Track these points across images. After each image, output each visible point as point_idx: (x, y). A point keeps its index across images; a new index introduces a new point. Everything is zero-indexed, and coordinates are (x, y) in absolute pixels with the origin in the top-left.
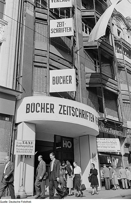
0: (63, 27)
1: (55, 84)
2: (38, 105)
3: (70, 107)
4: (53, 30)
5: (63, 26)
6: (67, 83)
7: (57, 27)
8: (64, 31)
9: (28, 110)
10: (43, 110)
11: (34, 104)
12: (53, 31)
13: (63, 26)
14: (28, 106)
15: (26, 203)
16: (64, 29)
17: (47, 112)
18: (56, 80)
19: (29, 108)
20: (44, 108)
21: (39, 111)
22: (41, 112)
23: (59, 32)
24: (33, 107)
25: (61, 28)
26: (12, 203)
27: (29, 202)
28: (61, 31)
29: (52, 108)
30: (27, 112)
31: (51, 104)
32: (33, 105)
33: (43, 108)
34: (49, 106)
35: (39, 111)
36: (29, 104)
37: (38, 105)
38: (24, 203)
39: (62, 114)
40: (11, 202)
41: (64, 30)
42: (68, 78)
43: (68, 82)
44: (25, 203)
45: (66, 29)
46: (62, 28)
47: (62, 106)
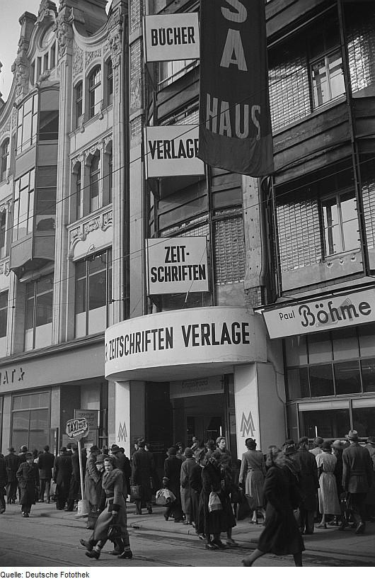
0: (181, 264)
1: (156, 44)
4: (156, 272)
5: (184, 261)
6: (184, 42)
7: (167, 261)
10: (132, 347)
12: (155, 275)
13: (184, 261)
14: (206, 328)
15: (75, 579)
16: (187, 270)
18: (158, 37)
23: (173, 280)
26: (35, 579)
27: (84, 574)
38: (68, 579)
40: (32, 575)
42: (186, 32)
43: (186, 39)
44: (71, 579)
45: (192, 268)
46: (180, 267)
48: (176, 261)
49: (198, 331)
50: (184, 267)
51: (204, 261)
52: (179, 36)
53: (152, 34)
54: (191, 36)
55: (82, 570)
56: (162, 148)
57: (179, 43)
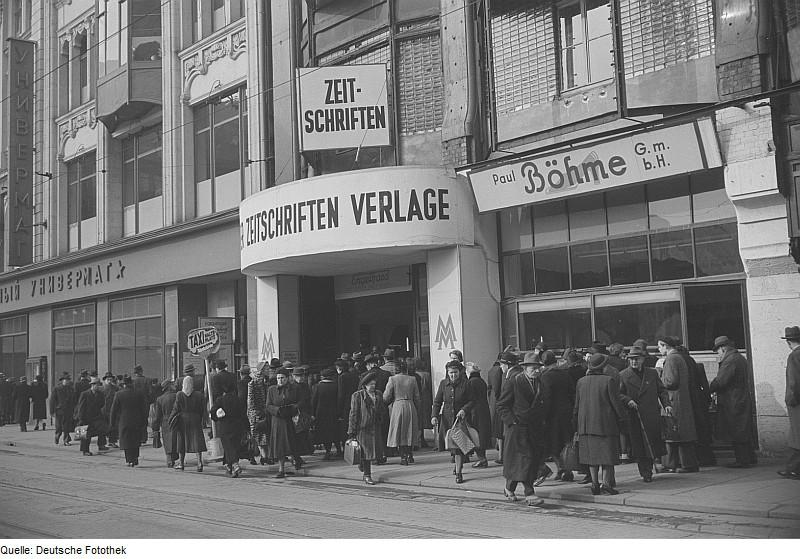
0: (350, 105)
4: (313, 118)
5: (353, 100)
7: (328, 101)
8: (358, 124)
10: (661, 162)
12: (311, 121)
13: (353, 100)
14: (386, 198)
15: (106, 556)
16: (357, 114)
23: (338, 129)
25: (343, 106)
26: (49, 556)
27: (118, 549)
28: (345, 123)
31: (382, 194)
36: (388, 194)
38: (97, 556)
40: (46, 550)
44: (101, 556)
45: (365, 112)
49: (375, 202)
50: (353, 110)
51: (382, 101)
55: (116, 543)
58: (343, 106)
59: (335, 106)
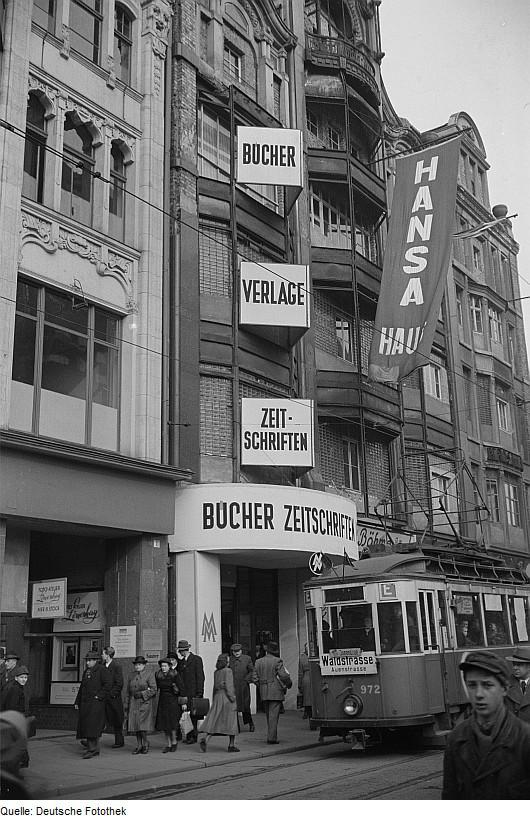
0: (281, 430)
2: (235, 507)
3: (308, 509)
5: (283, 427)
7: (263, 425)
8: (286, 446)
9: (209, 521)
10: (247, 521)
11: (225, 504)
12: (249, 440)
13: (283, 427)
14: (208, 508)
16: (286, 438)
17: (255, 301)
19: (213, 516)
20: (250, 517)
21: (238, 525)
22: (244, 527)
24: (221, 512)
25: (275, 430)
27: (118, 811)
29: (269, 514)
30: (206, 527)
31: (263, 282)
32: (221, 506)
33: (248, 517)
34: (261, 511)
35: (238, 525)
36: (211, 505)
37: (235, 507)
39: (290, 529)
40: (46, 812)
41: (284, 442)
42: (285, 151)
47: (290, 507)
48: (273, 426)
50: (283, 434)
52: (276, 155)
53: (245, 149)
54: (291, 157)
55: (116, 804)
56: (259, 290)
57: (276, 164)
58: (275, 430)
59: (269, 430)
